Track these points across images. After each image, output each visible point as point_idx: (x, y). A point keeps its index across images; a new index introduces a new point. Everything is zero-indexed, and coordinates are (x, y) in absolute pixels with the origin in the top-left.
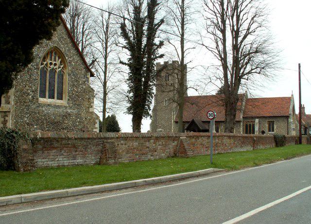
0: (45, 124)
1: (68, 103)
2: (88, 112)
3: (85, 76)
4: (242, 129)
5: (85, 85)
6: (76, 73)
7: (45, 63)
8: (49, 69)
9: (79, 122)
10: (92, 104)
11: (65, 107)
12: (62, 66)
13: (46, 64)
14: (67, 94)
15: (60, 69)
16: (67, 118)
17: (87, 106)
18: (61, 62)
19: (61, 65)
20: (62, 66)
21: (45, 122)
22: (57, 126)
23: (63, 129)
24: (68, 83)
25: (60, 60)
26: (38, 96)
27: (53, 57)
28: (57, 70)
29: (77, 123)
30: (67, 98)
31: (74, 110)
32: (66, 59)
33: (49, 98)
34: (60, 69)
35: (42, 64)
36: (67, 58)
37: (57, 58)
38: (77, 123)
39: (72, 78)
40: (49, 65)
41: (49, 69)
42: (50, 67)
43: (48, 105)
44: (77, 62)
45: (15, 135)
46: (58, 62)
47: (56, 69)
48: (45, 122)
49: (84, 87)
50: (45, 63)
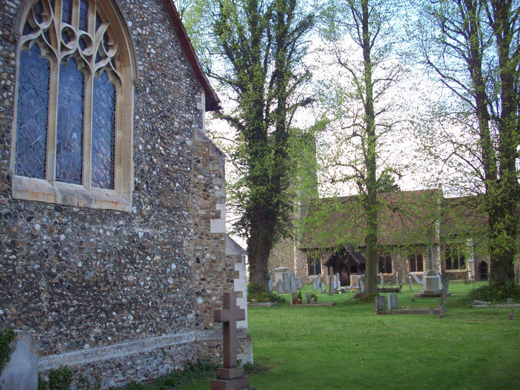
0: (44, 296)
1: (137, 202)
2: (204, 234)
3: (191, 101)
4: (439, 259)
5: (191, 136)
6: (160, 86)
7: (44, 26)
8: (60, 56)
9: (178, 275)
10: (218, 207)
11: (124, 214)
12: (111, 54)
13: (47, 33)
14: (133, 164)
15: (103, 64)
16: (133, 262)
17: (202, 212)
18: (106, 37)
19: (108, 48)
20: (111, 54)
21: (43, 284)
22: (95, 300)
23: (120, 307)
24: (136, 122)
25: (103, 28)
26: (12, 168)
27: (76, 11)
28: (94, 67)
29: (171, 281)
30: (133, 179)
31: (157, 227)
32: (125, 25)
33: (419, 271)
34: (103, 64)
35: (29, 29)
36: (130, 24)
37: (92, 19)
38: (171, 281)
39: (149, 104)
40: (60, 39)
41: (60, 56)
42: (63, 48)
43: (58, 208)
44: (162, 48)
45: (389, 173)
46: (97, 35)
47: (89, 58)
48: (43, 284)
49: (189, 142)
50: (44, 26)
